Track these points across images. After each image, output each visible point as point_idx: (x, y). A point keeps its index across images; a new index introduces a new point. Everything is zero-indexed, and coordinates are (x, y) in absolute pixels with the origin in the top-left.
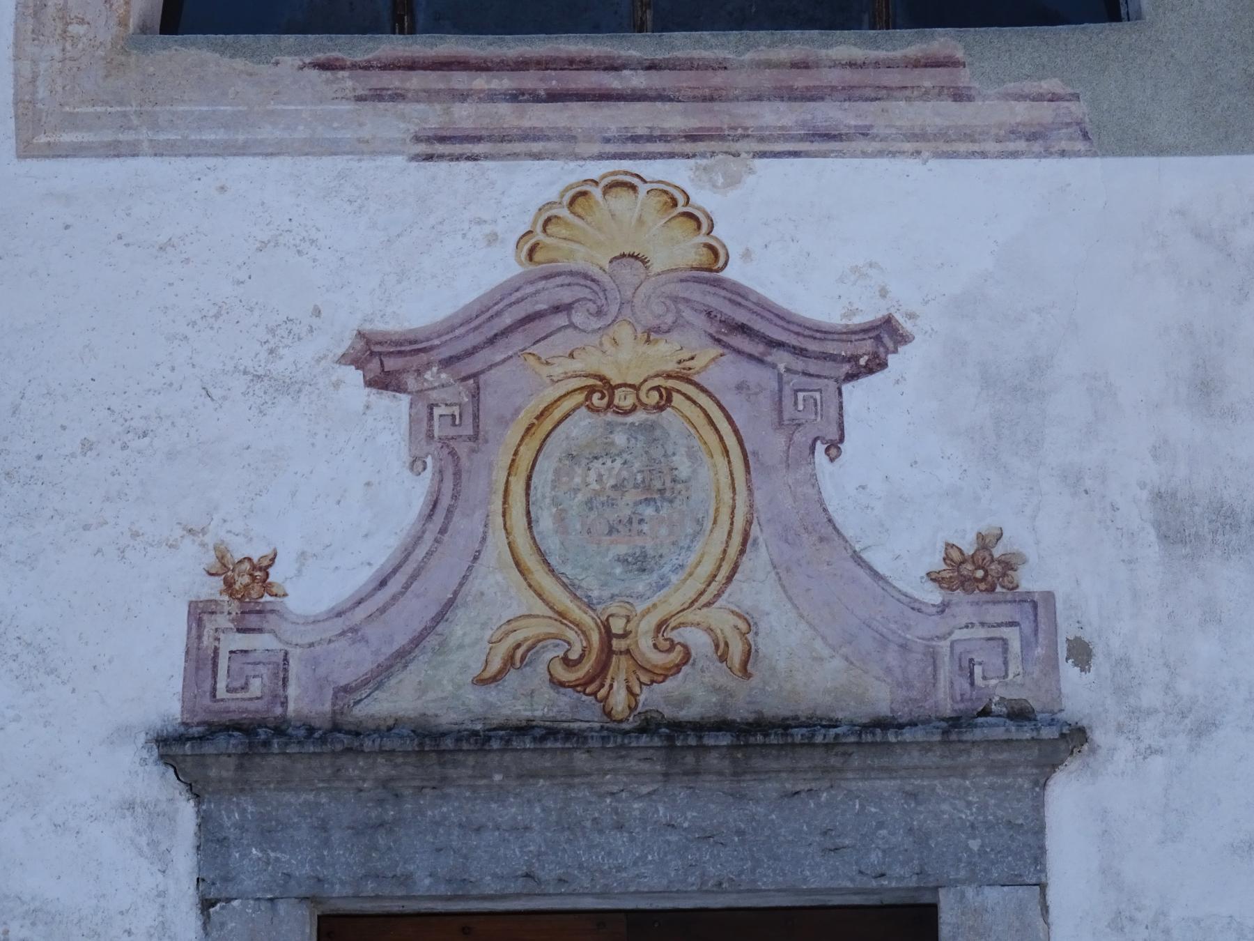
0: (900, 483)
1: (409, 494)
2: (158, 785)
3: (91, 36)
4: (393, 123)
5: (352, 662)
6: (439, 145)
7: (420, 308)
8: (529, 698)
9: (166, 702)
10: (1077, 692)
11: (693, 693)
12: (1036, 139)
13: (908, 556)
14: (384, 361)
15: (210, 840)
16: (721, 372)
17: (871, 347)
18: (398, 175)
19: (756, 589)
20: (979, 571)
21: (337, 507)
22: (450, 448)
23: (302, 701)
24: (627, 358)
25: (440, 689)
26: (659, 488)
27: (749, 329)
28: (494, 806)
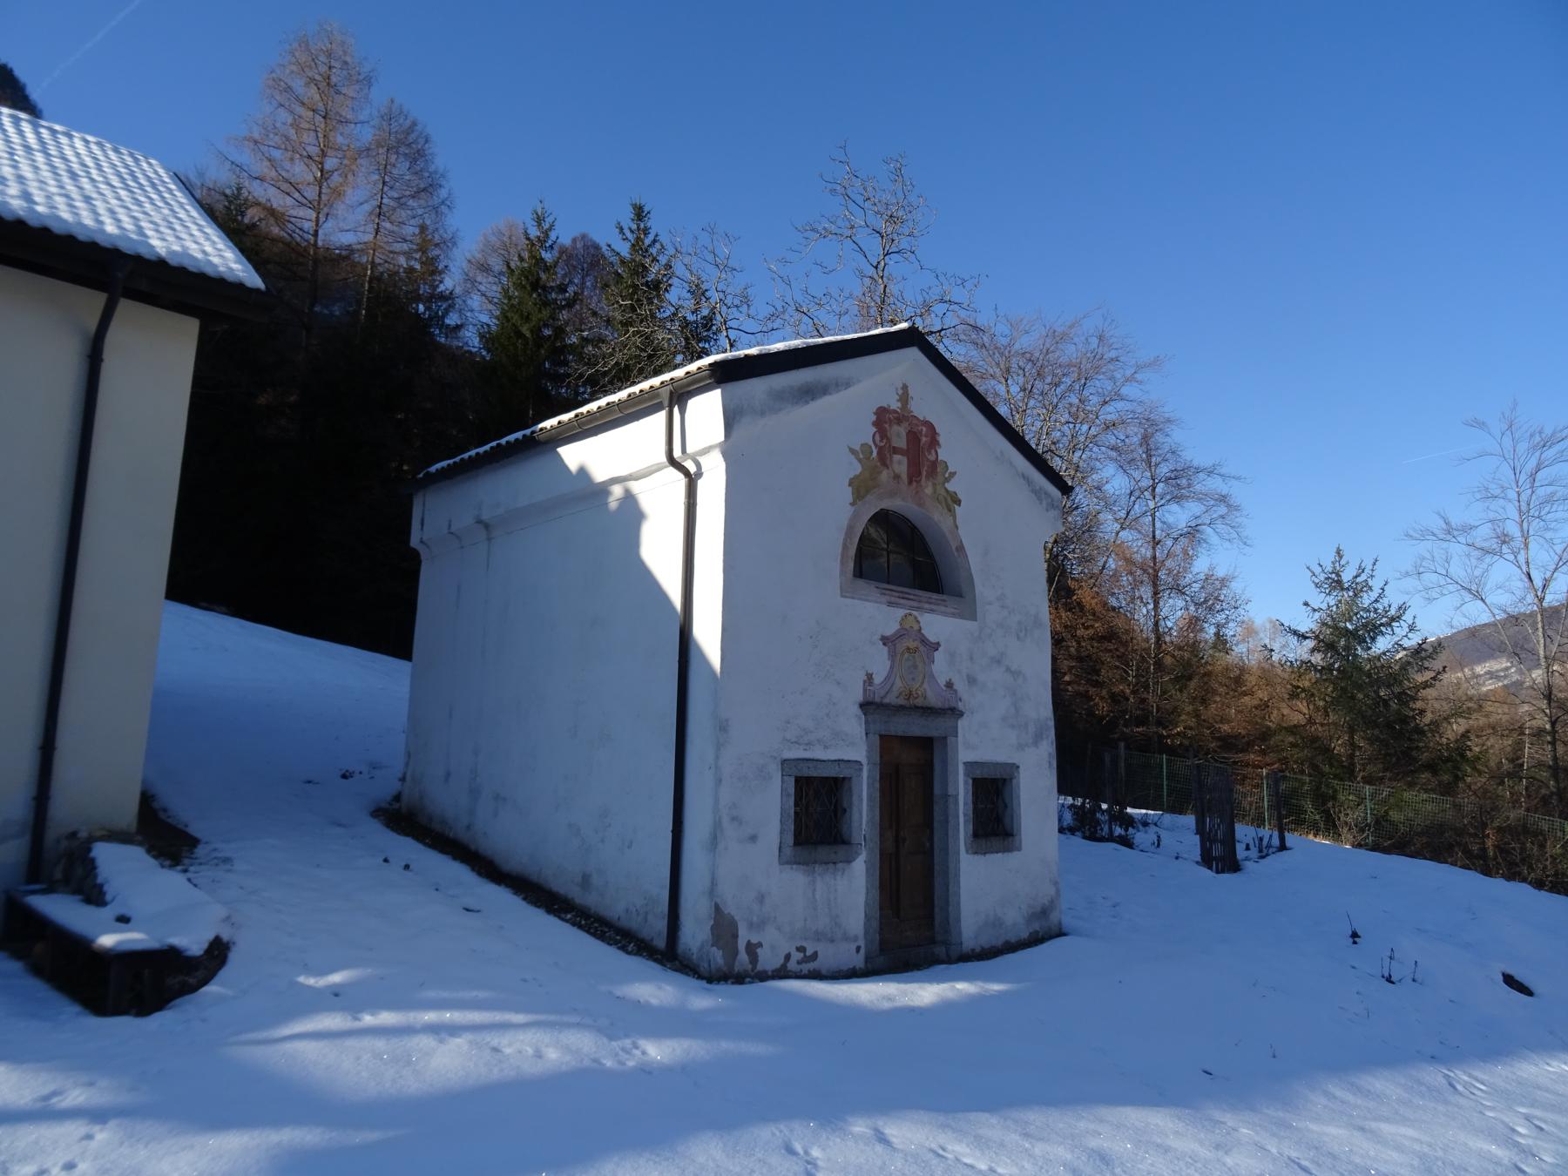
0: (941, 668)
1: (888, 663)
2: (859, 712)
3: (729, 301)
4: (884, 599)
5: (883, 693)
6: (890, 604)
7: (889, 632)
8: (901, 701)
9: (860, 698)
10: (961, 706)
11: (919, 702)
12: (954, 615)
13: (942, 682)
14: (885, 640)
15: (867, 722)
16: (922, 648)
17: (936, 647)
18: (885, 607)
19: (925, 685)
20: (949, 685)
22: (893, 656)
23: (877, 700)
24: (912, 645)
25: (891, 699)
26: (915, 667)
27: (924, 641)
28: (609, 1063)
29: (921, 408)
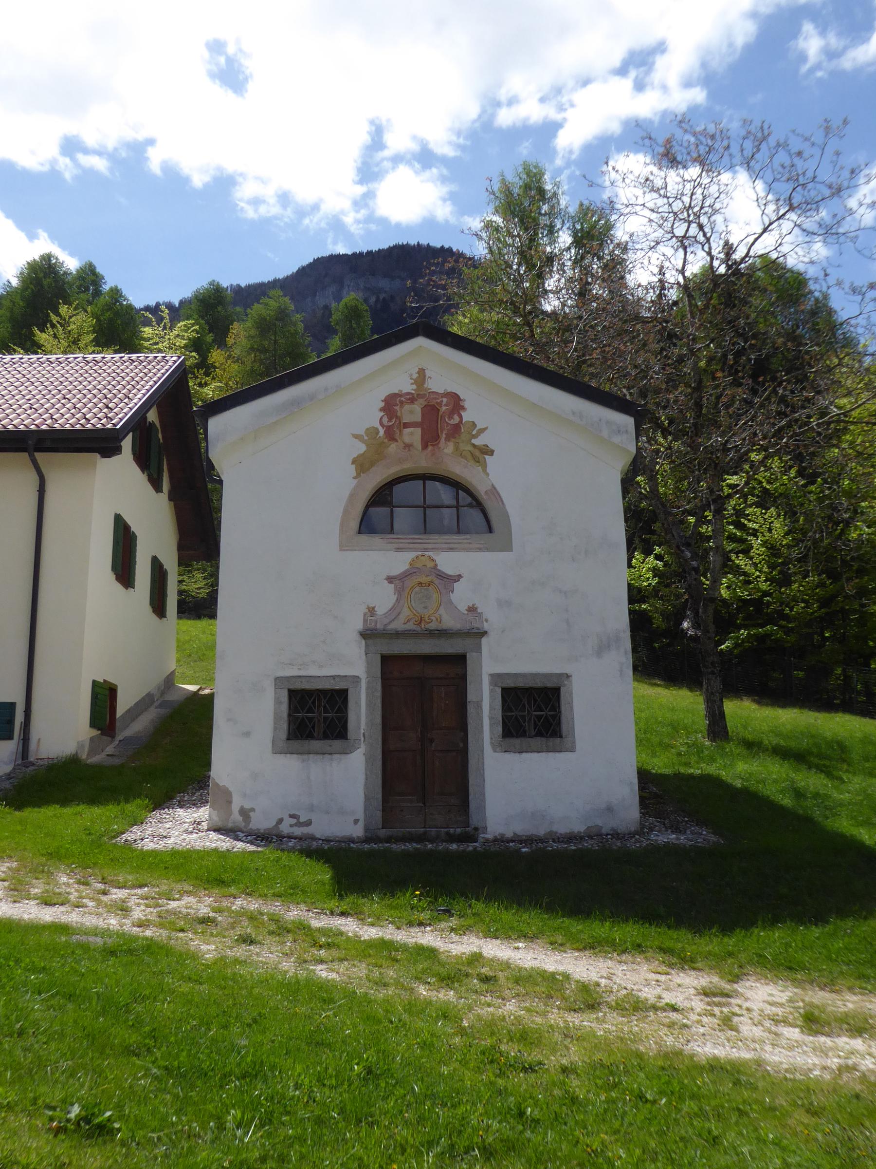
0: (462, 596)
21: (384, 599)
29: (438, 383)
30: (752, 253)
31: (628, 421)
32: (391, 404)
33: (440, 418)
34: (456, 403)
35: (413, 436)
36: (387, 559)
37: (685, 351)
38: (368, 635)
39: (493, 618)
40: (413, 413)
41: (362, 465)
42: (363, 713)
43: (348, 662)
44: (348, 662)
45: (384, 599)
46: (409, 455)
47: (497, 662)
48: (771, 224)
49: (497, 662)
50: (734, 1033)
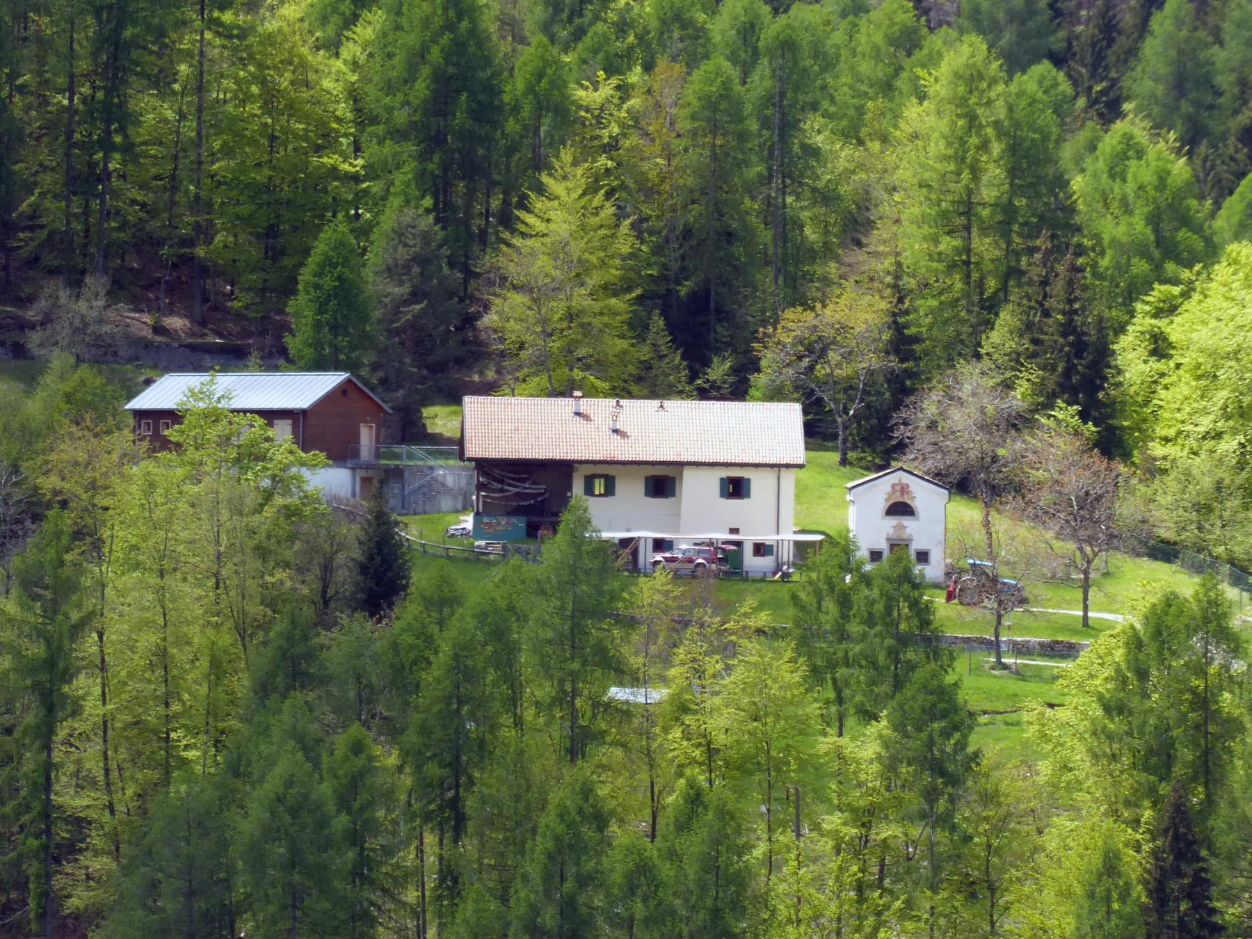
0: (908, 531)
21: (891, 531)
29: (904, 481)
30: (950, 526)
31: (1131, 361)
32: (893, 486)
33: (904, 489)
34: (908, 486)
35: (898, 494)
36: (893, 521)
37: (616, 130)
38: (888, 539)
39: (915, 537)
40: (898, 488)
41: (887, 500)
42: (886, 554)
43: (883, 545)
44: (883, 545)
45: (891, 531)
46: (897, 498)
47: (916, 546)
48: (992, 916)
49: (916, 546)
50: (1061, 681)
